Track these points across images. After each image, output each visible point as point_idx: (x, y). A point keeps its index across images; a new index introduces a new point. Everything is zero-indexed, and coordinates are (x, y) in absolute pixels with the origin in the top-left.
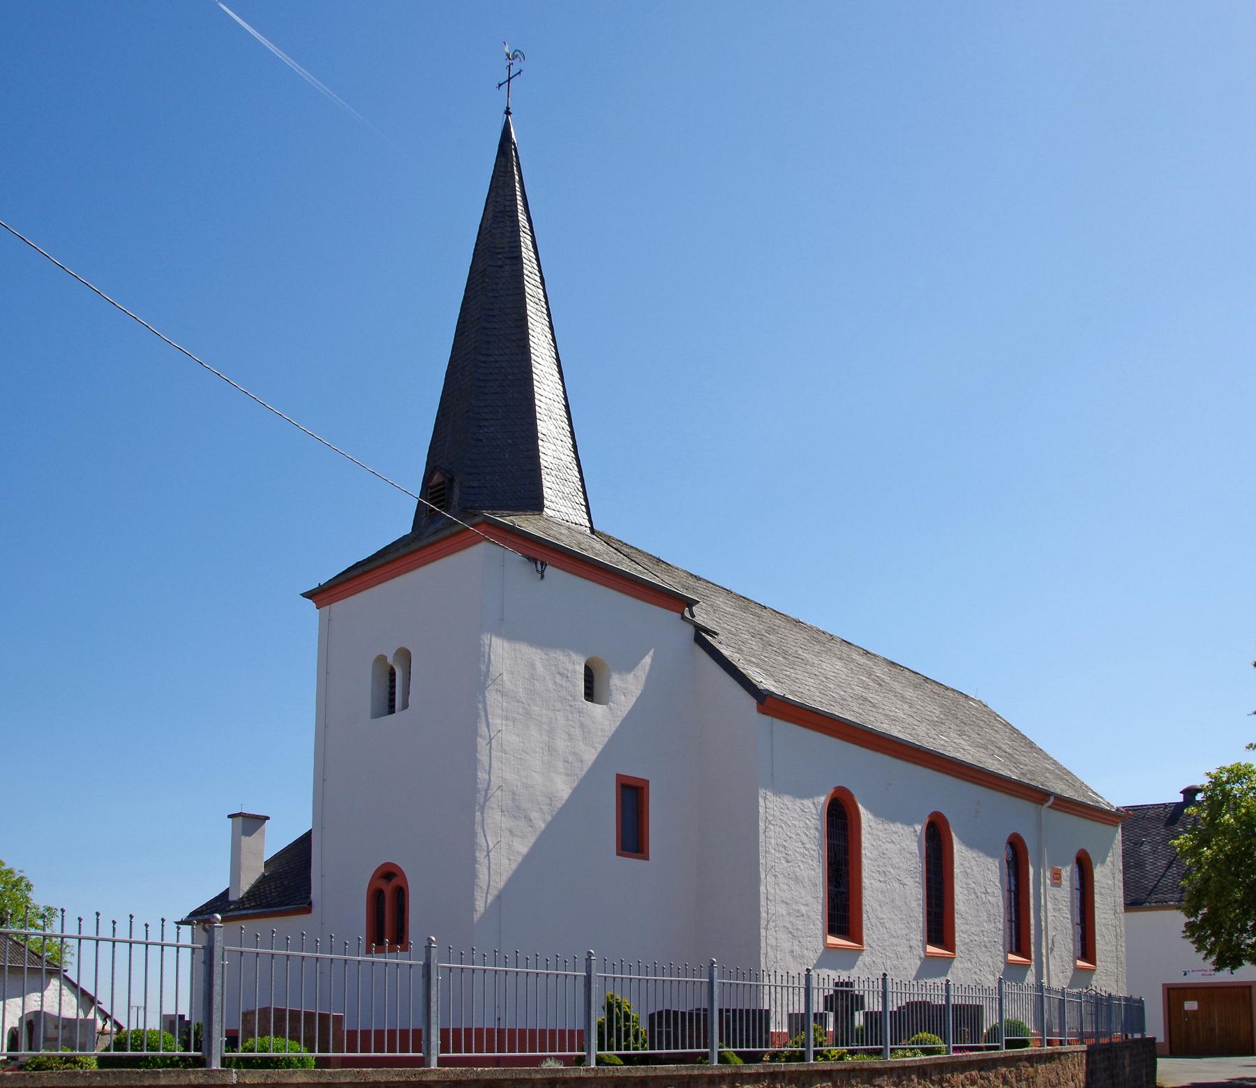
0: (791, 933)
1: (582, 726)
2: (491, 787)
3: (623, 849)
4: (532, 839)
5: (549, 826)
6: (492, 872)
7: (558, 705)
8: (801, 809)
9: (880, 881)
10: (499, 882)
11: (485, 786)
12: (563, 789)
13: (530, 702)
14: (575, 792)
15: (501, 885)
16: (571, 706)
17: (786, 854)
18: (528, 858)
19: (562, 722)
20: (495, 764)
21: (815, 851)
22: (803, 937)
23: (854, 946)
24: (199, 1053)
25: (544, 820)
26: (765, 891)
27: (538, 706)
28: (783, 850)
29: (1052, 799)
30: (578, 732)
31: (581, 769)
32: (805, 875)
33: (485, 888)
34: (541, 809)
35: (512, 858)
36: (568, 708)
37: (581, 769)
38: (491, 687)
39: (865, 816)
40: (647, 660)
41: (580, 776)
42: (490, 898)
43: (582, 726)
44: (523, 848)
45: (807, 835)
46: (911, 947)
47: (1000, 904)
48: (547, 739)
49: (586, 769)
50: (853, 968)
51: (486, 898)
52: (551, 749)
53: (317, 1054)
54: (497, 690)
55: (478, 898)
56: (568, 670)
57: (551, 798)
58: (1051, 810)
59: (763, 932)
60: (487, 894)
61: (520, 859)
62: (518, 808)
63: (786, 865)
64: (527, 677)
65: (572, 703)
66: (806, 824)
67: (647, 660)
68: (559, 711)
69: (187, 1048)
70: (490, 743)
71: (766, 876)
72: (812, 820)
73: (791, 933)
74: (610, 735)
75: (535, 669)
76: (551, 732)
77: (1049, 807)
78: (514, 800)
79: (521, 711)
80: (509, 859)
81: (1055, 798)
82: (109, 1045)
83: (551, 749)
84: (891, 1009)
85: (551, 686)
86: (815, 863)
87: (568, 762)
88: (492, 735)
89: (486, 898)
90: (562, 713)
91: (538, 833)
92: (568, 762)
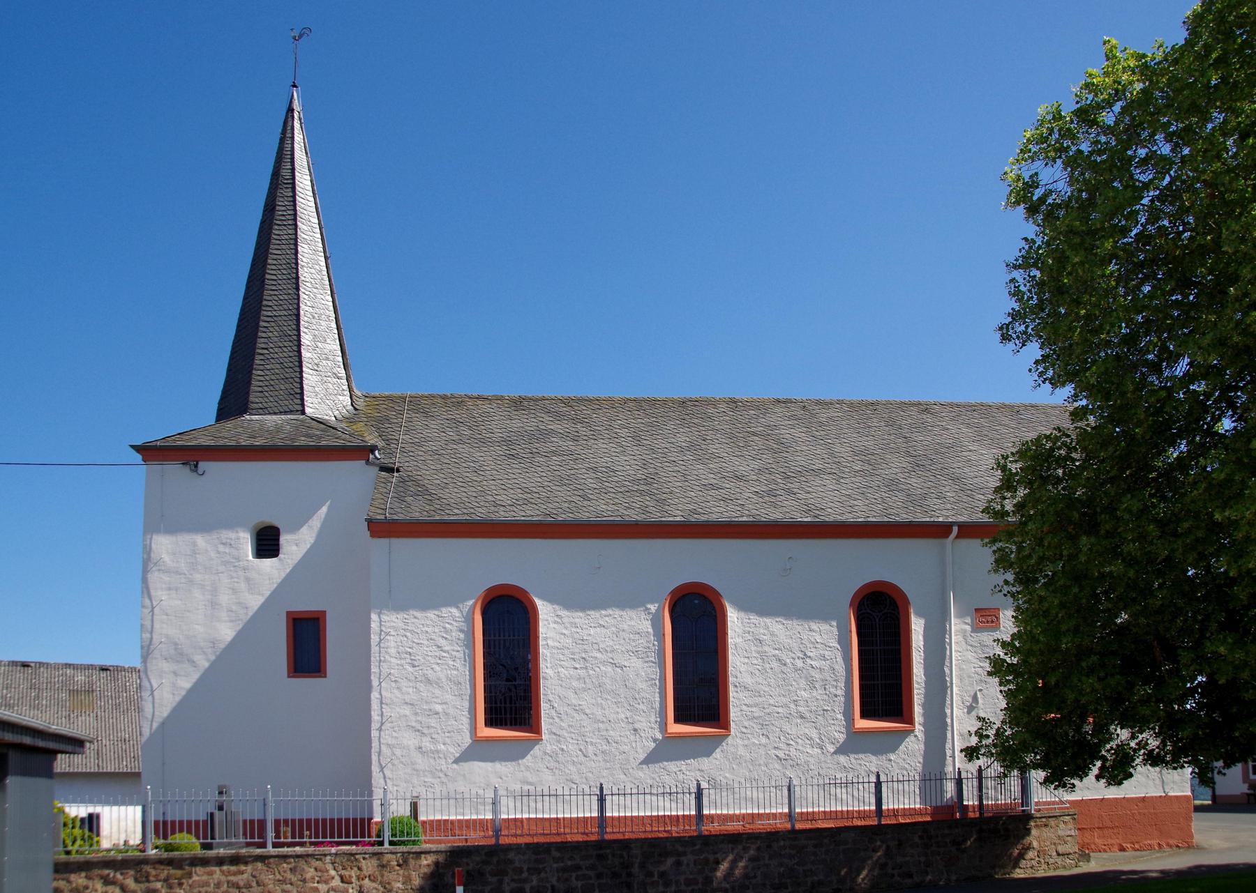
0: (419, 731)
1: (248, 580)
2: (153, 642)
3: (319, 671)
4: (195, 676)
5: (213, 665)
6: (156, 705)
7: (221, 568)
8: (438, 616)
9: (576, 668)
10: (164, 712)
11: (148, 643)
12: (227, 633)
13: (192, 572)
14: (239, 635)
15: (165, 714)
16: (235, 566)
17: (412, 660)
18: (191, 692)
19: (226, 581)
20: (157, 626)
21: (458, 651)
22: (438, 733)
23: (895, 727)
24: (261, 840)
25: (208, 660)
26: (378, 696)
27: (200, 573)
28: (408, 656)
29: (955, 529)
30: (243, 586)
31: (246, 614)
32: (442, 676)
33: (150, 717)
34: (203, 652)
35: (176, 693)
36: (232, 569)
37: (246, 614)
38: (154, 569)
39: (539, 603)
40: (324, 509)
41: (245, 621)
42: (155, 725)
43: (248, 580)
44: (186, 684)
45: (446, 638)
46: (635, 730)
47: (837, 667)
48: (210, 597)
49: (251, 614)
50: (523, 757)
51: (151, 725)
52: (214, 605)
53: (201, 841)
54: (159, 570)
55: (145, 725)
56: (231, 539)
57: (214, 643)
58: (958, 541)
59: (374, 734)
60: (152, 721)
61: (183, 693)
62: (181, 654)
63: (410, 669)
64: (189, 553)
65: (237, 564)
66: (445, 628)
67: (324, 509)
68: (222, 573)
69: (426, 836)
70: (152, 611)
71: (380, 683)
72: (454, 623)
73: (419, 731)
74: (279, 581)
75: (197, 546)
76: (215, 591)
77: (957, 537)
78: (176, 649)
79: (183, 581)
80: (174, 694)
81: (959, 526)
82: (1199, 848)
83: (214, 605)
84: (1036, 800)
85: (213, 555)
86: (458, 664)
87: (232, 611)
88: (155, 604)
89: (151, 725)
90: (225, 574)
91: (202, 671)
92: (232, 611)
